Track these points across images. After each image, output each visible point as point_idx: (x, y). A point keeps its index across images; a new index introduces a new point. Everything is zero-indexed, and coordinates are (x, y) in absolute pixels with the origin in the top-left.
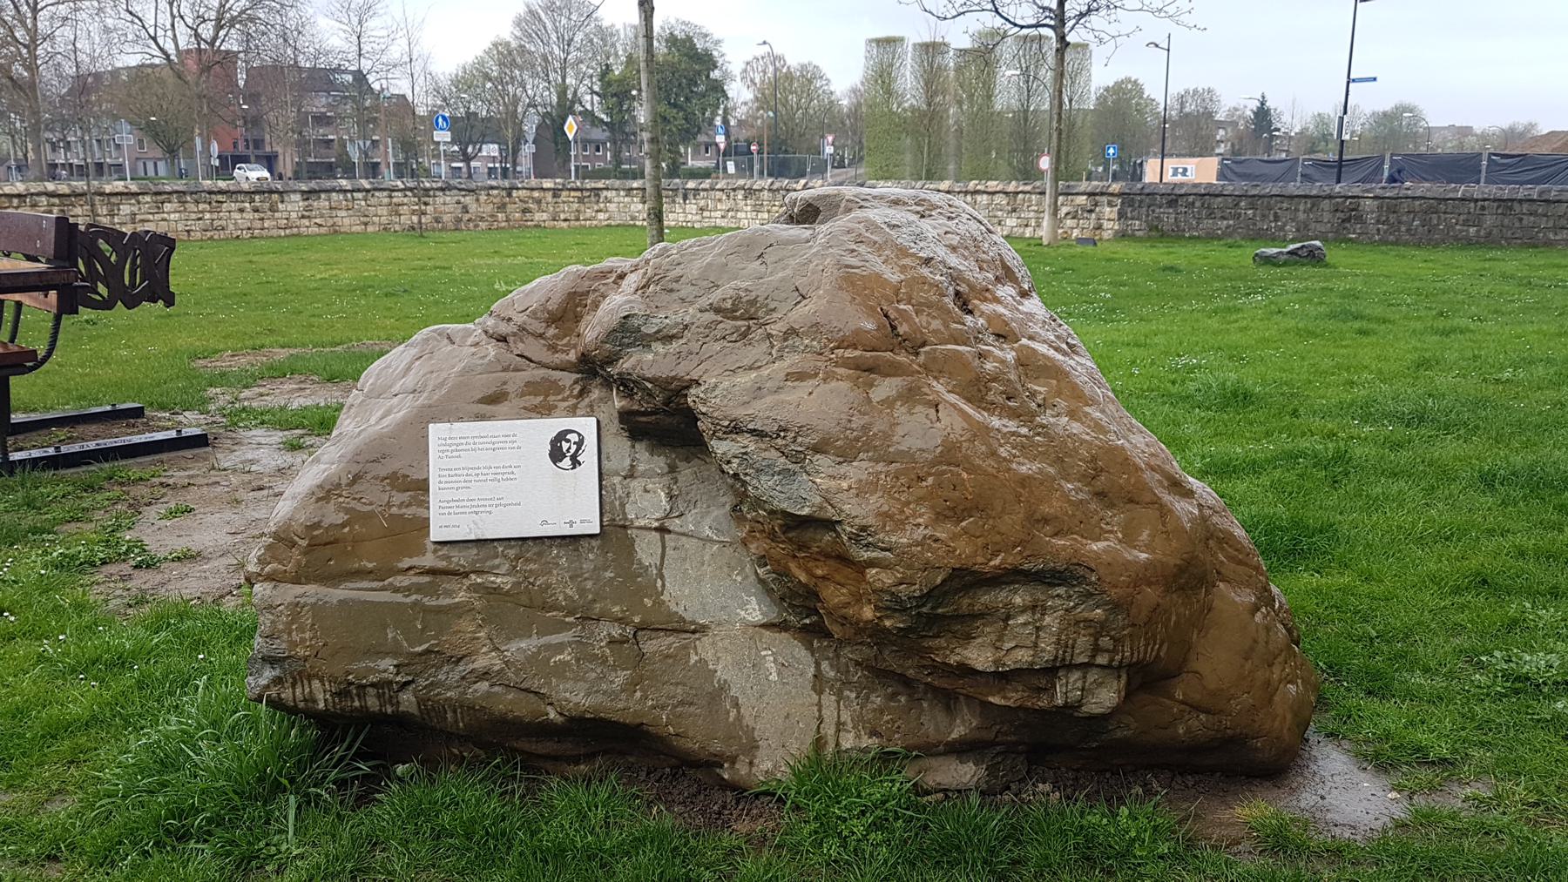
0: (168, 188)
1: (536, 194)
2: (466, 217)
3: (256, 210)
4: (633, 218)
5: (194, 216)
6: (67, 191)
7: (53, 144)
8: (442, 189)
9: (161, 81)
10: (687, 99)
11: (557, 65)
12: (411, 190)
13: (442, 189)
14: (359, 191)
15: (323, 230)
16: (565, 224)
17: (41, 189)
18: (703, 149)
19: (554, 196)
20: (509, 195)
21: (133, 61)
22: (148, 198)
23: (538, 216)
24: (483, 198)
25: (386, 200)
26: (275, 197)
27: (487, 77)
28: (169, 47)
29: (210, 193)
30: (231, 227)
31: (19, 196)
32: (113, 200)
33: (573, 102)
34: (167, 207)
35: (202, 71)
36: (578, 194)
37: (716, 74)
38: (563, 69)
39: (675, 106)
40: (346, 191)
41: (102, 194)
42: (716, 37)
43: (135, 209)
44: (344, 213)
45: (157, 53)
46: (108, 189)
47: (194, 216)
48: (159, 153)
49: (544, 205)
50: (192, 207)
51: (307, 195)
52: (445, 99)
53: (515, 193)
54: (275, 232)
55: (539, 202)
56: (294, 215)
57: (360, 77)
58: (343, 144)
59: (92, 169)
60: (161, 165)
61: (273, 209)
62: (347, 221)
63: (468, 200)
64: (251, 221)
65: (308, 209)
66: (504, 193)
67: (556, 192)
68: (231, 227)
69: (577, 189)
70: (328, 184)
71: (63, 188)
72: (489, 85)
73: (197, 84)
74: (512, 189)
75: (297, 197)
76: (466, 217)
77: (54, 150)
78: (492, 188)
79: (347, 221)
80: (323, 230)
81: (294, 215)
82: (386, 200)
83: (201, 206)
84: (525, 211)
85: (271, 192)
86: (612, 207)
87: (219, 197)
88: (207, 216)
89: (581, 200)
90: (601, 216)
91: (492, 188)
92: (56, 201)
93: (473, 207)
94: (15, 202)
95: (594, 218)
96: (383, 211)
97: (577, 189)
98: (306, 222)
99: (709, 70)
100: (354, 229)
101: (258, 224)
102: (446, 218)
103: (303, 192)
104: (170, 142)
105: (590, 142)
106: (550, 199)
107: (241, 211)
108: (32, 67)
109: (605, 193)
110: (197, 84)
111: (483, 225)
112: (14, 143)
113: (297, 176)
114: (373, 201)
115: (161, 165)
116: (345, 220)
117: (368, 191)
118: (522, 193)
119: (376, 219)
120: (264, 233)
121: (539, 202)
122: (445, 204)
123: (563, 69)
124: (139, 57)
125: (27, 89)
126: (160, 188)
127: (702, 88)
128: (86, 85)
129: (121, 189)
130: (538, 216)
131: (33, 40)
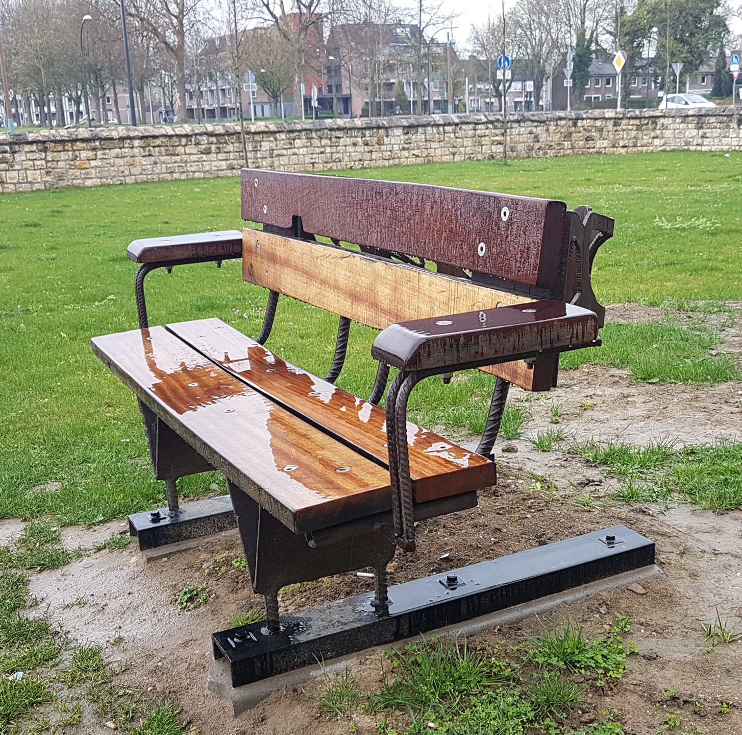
0: (298, 127)
1: (598, 123)
2: (537, 146)
3: (367, 144)
4: (687, 144)
5: (317, 150)
6: (223, 131)
7: (191, 94)
8: (518, 121)
9: (270, 41)
10: (692, 34)
11: (578, 11)
12: (492, 122)
13: (518, 121)
14: (449, 124)
15: (419, 160)
16: (623, 151)
17: (203, 130)
18: (700, 79)
19: (615, 125)
20: (575, 125)
21: (251, 25)
22: (283, 136)
23: (600, 144)
24: (552, 128)
25: (471, 133)
26: (382, 132)
27: (518, 24)
28: (278, 12)
29: (331, 130)
30: (346, 159)
31: (186, 136)
32: (257, 138)
33: (590, 41)
34: (298, 143)
35: (301, 30)
36: (637, 122)
37: (718, 11)
38: (583, 12)
39: (682, 41)
40: (439, 125)
41: (248, 133)
42: (445, 11)
43: (273, 145)
44: (436, 145)
45: (270, 17)
46: (253, 129)
47: (317, 150)
48: (265, 98)
49: (605, 133)
50: (316, 142)
51: (409, 129)
52: (483, 46)
53: (580, 123)
54: (380, 163)
55: (601, 130)
56: (396, 147)
57: (417, 31)
58: (401, 86)
59: (217, 112)
60: (267, 107)
61: (380, 143)
62: (438, 152)
63: (540, 130)
64: (362, 153)
65: (408, 142)
66: (571, 123)
67: (616, 121)
68: (346, 159)
69: (636, 118)
70: (425, 119)
71: (220, 129)
72: (519, 31)
73: (298, 40)
74: (577, 119)
75: (398, 132)
76: (537, 146)
77: (191, 98)
78: (561, 119)
79: (438, 152)
80: (419, 160)
81: (396, 147)
82: (471, 133)
83: (324, 142)
84: (587, 139)
85: (379, 128)
86: (667, 133)
87: (338, 134)
88: (328, 150)
89: (639, 128)
90: (657, 142)
91: (561, 119)
92: (214, 139)
93: (543, 137)
94: (184, 141)
95: (650, 144)
96: (468, 142)
97: (636, 118)
98: (406, 153)
99: (712, 7)
100: (444, 158)
101: (367, 156)
102: (520, 147)
103: (404, 127)
104: (274, 88)
105: (602, 76)
106: (610, 127)
107: (355, 144)
108: (180, 33)
109: (662, 120)
110: (298, 40)
111: (551, 153)
112: (164, 93)
113: (365, 114)
114: (460, 134)
115: (267, 108)
116: (439, 152)
117: (456, 125)
118: (586, 123)
119: (462, 149)
120: (373, 164)
121: (601, 130)
122: (520, 134)
123: (583, 12)
124: (256, 21)
125: (177, 51)
126: (293, 127)
127: (706, 23)
128: (212, 48)
129: (263, 129)
130: (600, 144)
131: (181, 12)
